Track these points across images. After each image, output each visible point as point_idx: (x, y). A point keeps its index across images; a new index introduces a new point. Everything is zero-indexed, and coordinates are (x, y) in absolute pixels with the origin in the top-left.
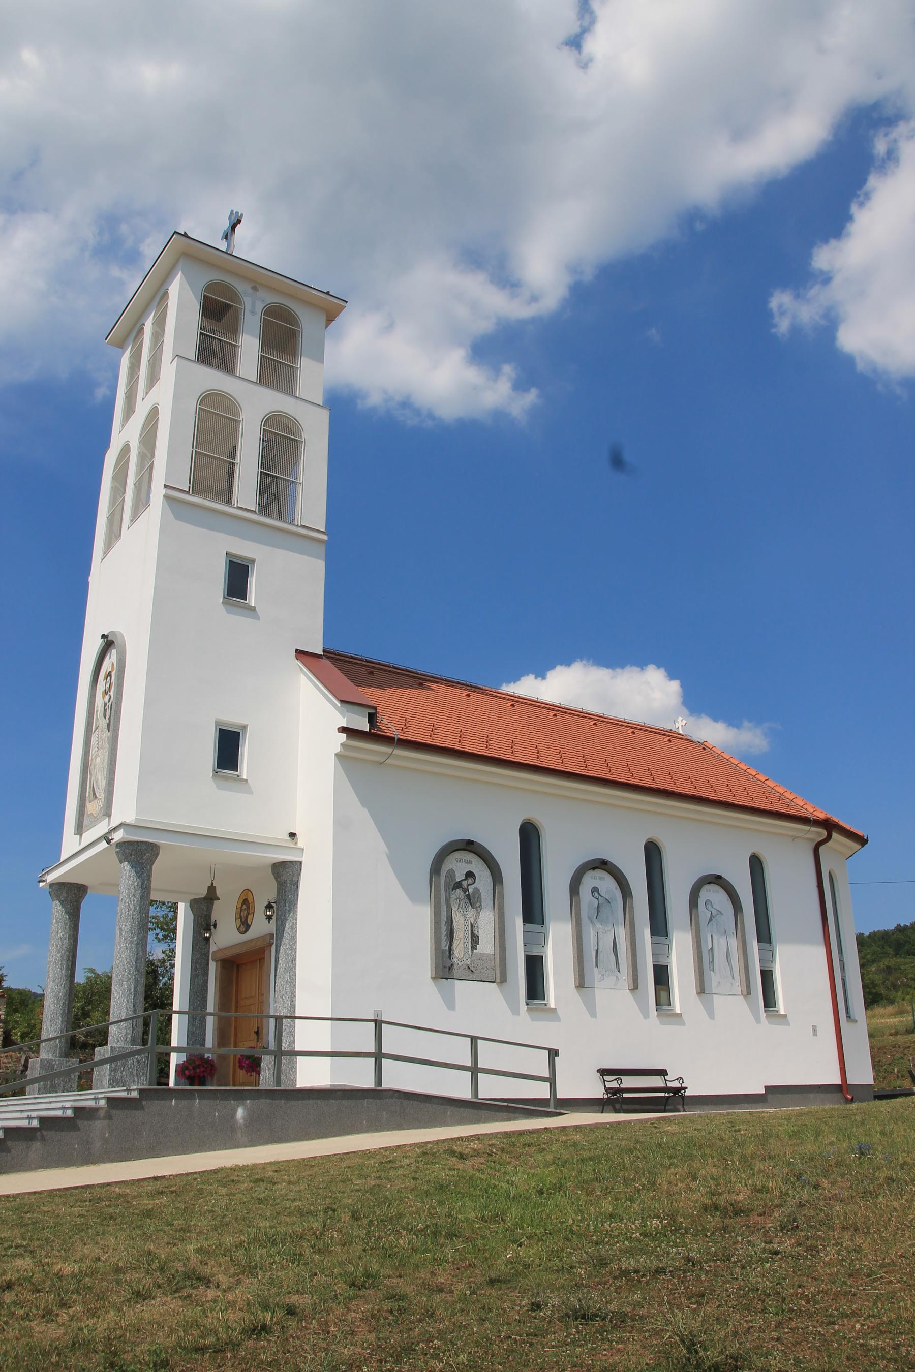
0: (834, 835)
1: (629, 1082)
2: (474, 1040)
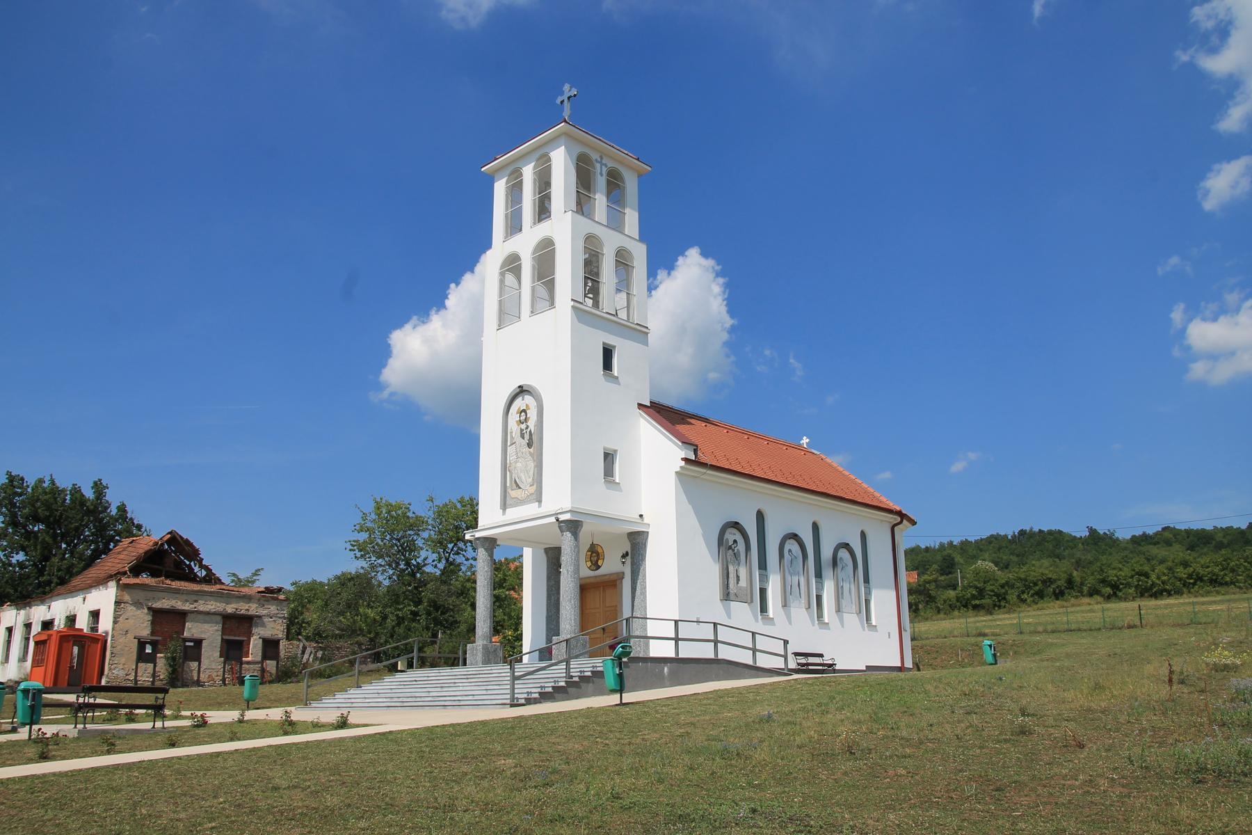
2: (754, 634)
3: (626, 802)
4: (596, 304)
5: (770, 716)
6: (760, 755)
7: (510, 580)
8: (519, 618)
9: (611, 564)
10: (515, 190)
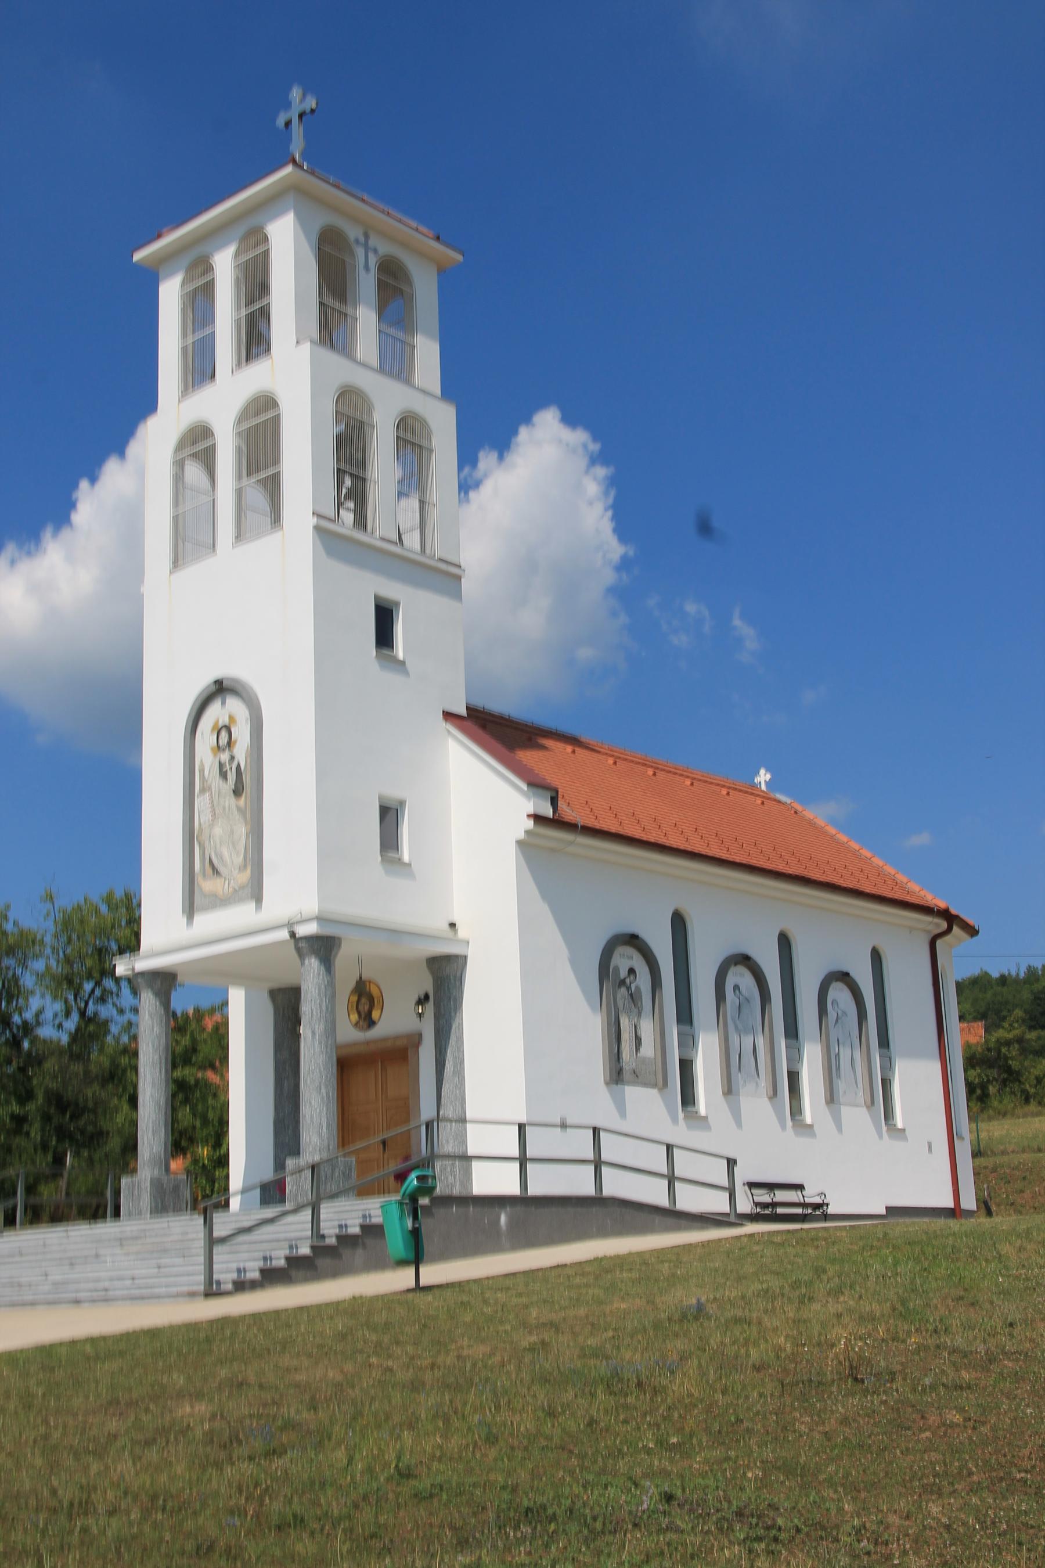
0: (955, 928)
1: (781, 1196)
3: (424, 1484)
4: (361, 521)
5: (700, 1307)
6: (683, 1385)
7: (205, 1050)
8: (223, 1123)
9: (396, 1018)
10: (199, 303)
